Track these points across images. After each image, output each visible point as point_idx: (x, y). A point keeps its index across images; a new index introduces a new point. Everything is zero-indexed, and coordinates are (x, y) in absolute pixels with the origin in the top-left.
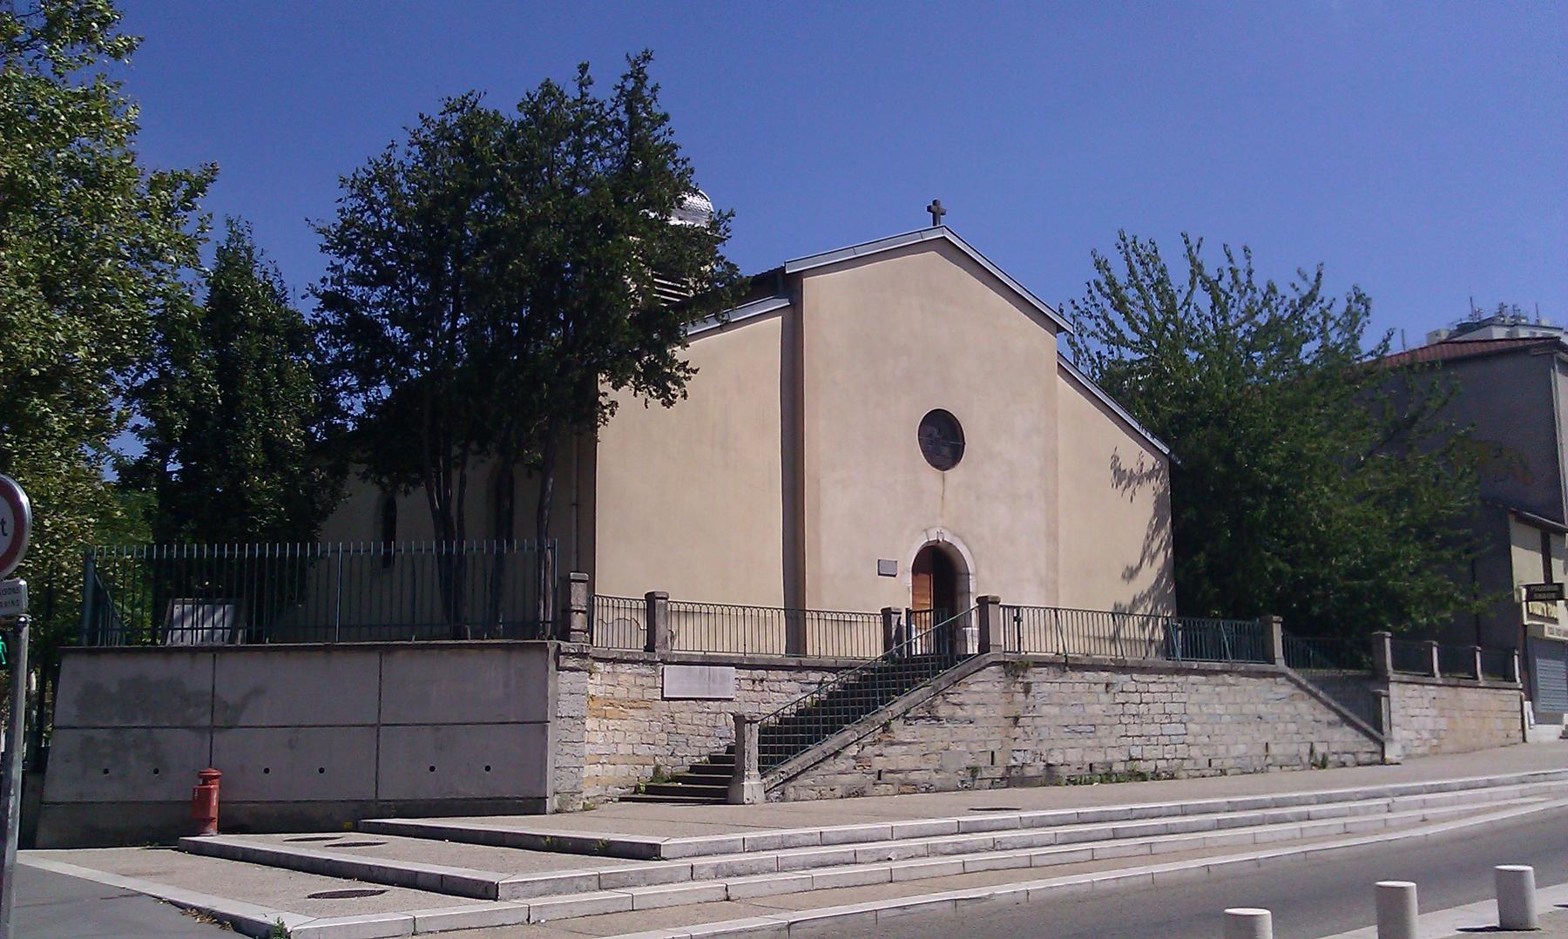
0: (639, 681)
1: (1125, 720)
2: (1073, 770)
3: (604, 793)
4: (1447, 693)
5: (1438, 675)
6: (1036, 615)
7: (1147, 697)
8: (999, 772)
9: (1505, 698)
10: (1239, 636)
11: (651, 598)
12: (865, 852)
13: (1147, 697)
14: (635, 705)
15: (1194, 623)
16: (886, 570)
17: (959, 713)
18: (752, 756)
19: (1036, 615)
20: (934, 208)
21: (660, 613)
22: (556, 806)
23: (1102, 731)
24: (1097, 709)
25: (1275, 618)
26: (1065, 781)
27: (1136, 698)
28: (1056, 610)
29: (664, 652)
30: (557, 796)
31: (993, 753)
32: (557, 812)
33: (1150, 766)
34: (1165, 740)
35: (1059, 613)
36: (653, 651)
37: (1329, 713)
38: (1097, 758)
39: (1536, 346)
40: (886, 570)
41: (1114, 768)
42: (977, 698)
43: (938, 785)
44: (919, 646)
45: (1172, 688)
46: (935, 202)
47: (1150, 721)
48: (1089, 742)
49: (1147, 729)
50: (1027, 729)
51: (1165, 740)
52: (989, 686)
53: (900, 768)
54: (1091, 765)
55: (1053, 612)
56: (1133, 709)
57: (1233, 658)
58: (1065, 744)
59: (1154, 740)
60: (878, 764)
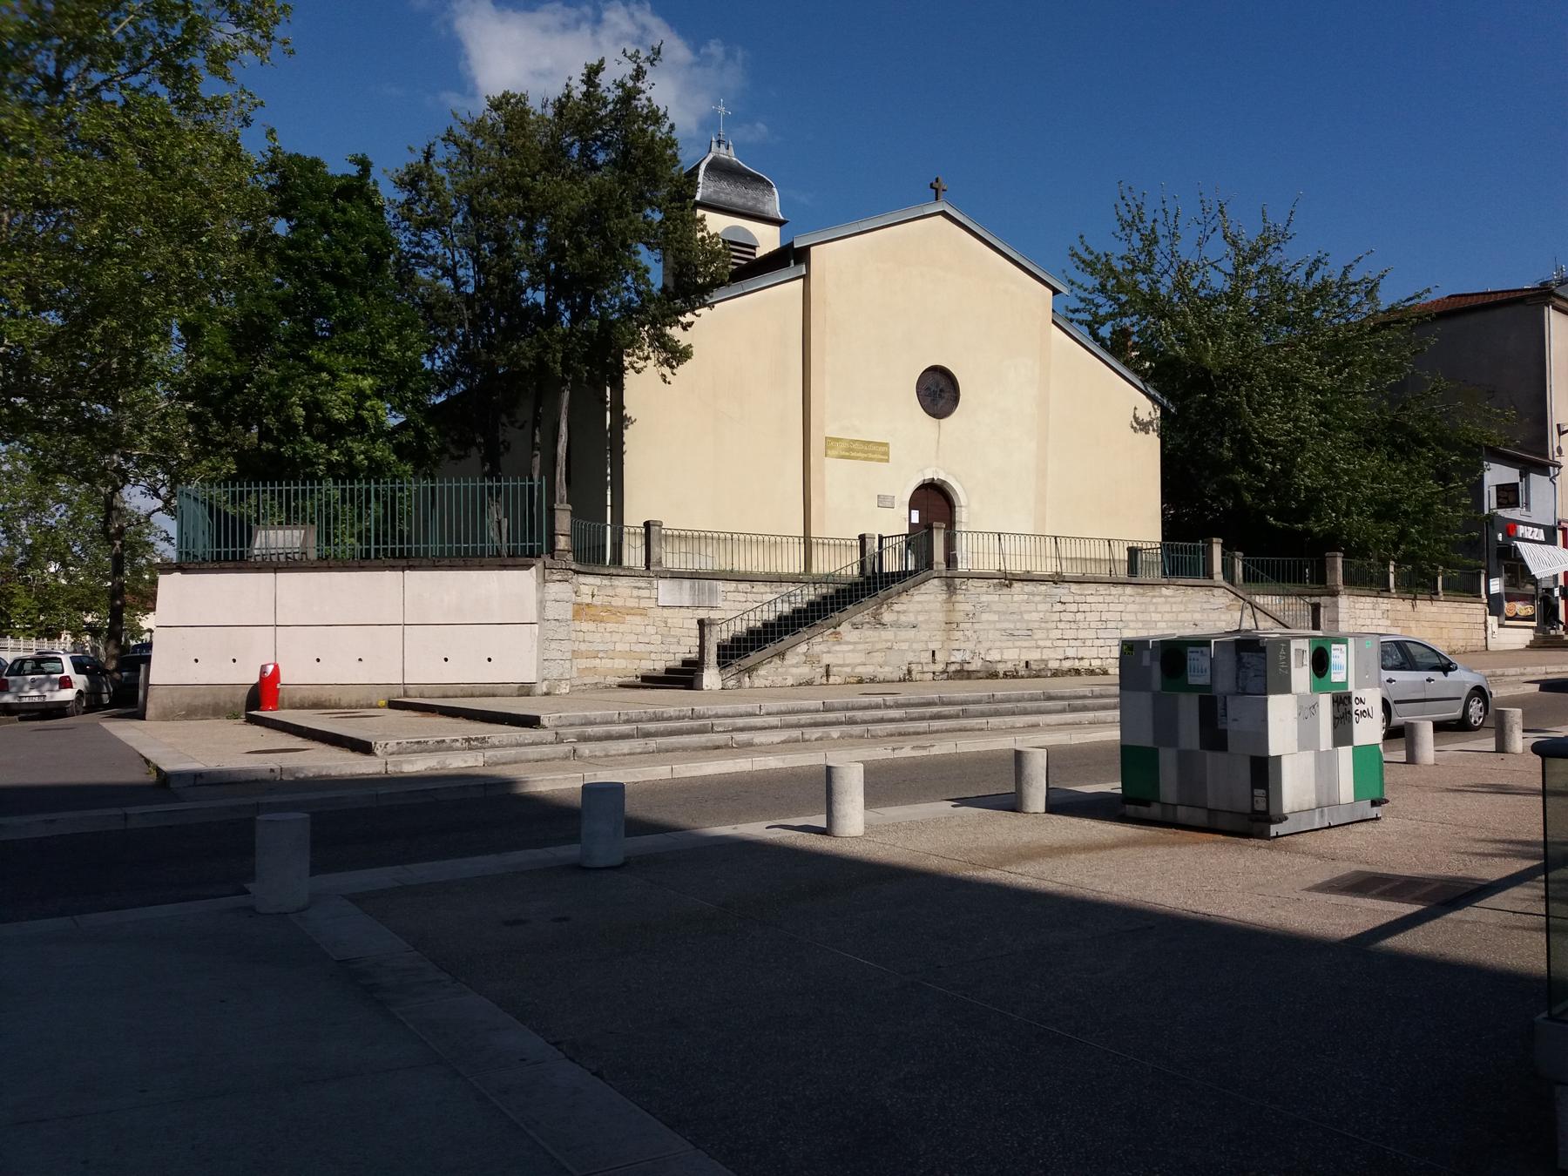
0: (636, 592)
1: (1060, 625)
2: (1010, 666)
3: (602, 681)
4: (1405, 606)
5: (1393, 591)
6: (970, 540)
7: (1083, 607)
8: (939, 667)
9: (1467, 611)
10: (1192, 556)
11: (647, 525)
12: (720, 725)
13: (1083, 607)
14: (632, 612)
15: (585, 526)
16: (884, 502)
17: (903, 618)
18: (712, 652)
19: (970, 540)
20: (936, 185)
21: (654, 536)
22: (545, 690)
23: (1039, 635)
24: (1035, 616)
25: (1215, 540)
26: (1001, 675)
27: (1074, 607)
28: (1056, 538)
29: (658, 569)
30: (546, 682)
31: (934, 652)
32: (547, 694)
33: (1085, 664)
34: (1100, 642)
35: (1002, 536)
36: (651, 568)
37: (1266, 621)
38: (1033, 656)
39: (1531, 296)
40: (884, 502)
41: (1050, 666)
42: (919, 607)
43: (881, 677)
44: (891, 564)
45: (1108, 599)
46: (937, 180)
47: (1087, 626)
48: (1026, 644)
49: (1082, 634)
50: (966, 633)
51: (1100, 642)
52: (932, 597)
53: (847, 662)
54: (1027, 662)
55: (1053, 539)
56: (1070, 617)
57: (1311, 582)
58: (1004, 645)
59: (1089, 643)
60: (826, 659)
